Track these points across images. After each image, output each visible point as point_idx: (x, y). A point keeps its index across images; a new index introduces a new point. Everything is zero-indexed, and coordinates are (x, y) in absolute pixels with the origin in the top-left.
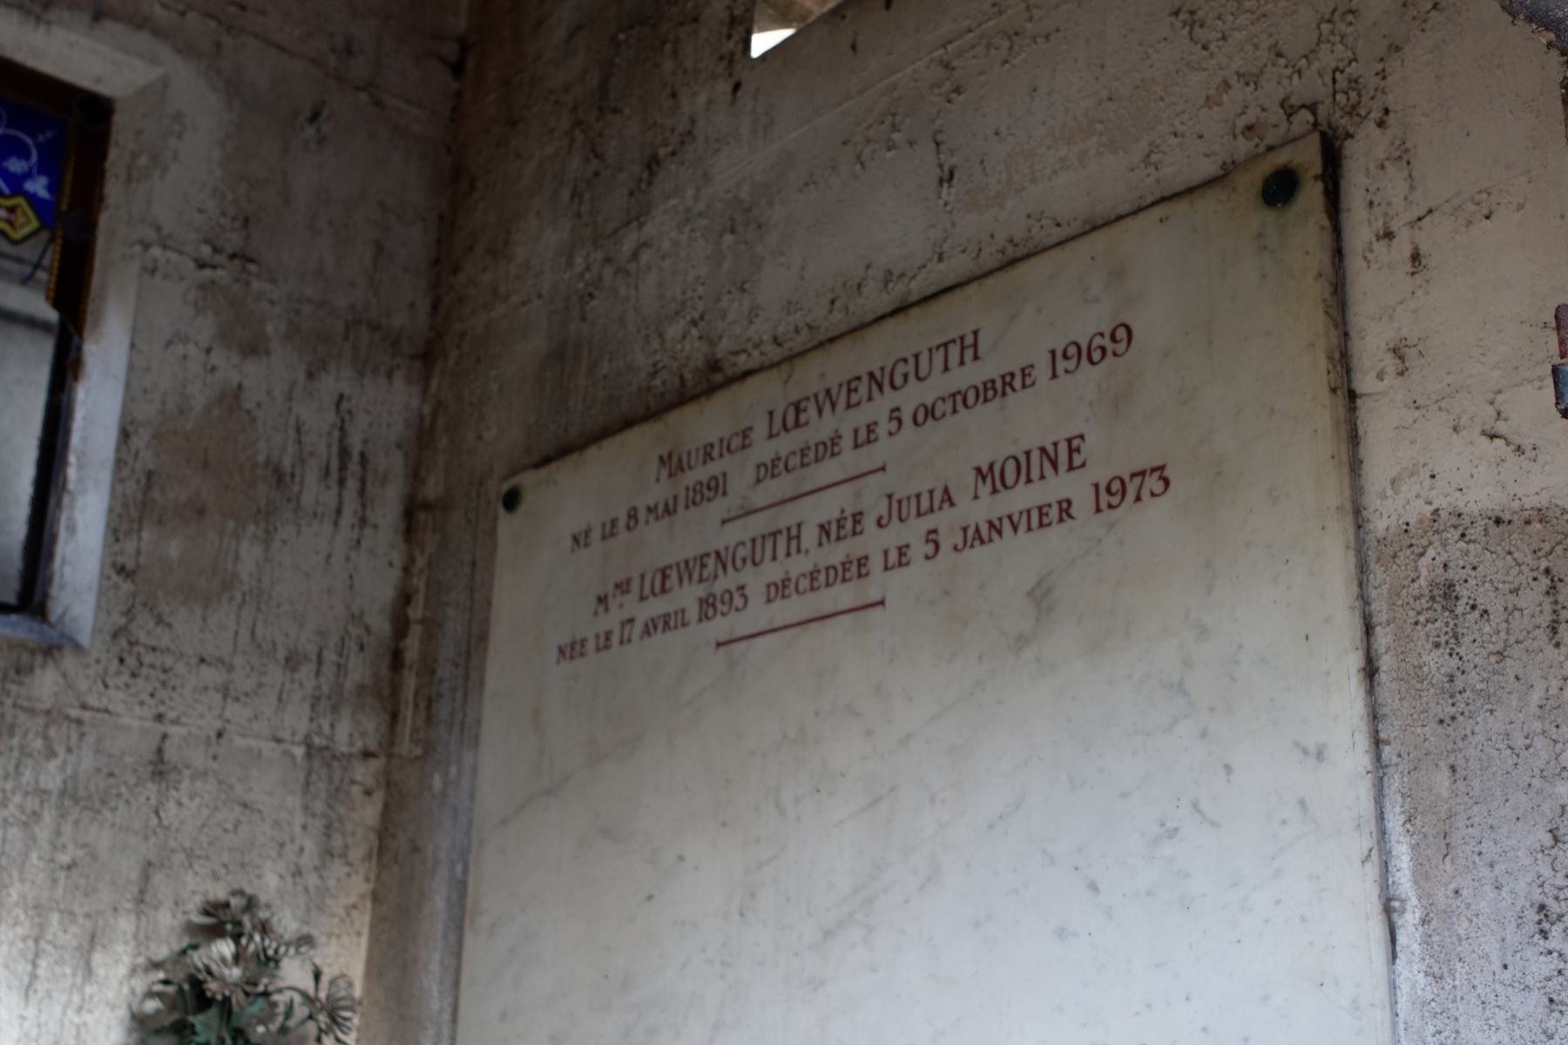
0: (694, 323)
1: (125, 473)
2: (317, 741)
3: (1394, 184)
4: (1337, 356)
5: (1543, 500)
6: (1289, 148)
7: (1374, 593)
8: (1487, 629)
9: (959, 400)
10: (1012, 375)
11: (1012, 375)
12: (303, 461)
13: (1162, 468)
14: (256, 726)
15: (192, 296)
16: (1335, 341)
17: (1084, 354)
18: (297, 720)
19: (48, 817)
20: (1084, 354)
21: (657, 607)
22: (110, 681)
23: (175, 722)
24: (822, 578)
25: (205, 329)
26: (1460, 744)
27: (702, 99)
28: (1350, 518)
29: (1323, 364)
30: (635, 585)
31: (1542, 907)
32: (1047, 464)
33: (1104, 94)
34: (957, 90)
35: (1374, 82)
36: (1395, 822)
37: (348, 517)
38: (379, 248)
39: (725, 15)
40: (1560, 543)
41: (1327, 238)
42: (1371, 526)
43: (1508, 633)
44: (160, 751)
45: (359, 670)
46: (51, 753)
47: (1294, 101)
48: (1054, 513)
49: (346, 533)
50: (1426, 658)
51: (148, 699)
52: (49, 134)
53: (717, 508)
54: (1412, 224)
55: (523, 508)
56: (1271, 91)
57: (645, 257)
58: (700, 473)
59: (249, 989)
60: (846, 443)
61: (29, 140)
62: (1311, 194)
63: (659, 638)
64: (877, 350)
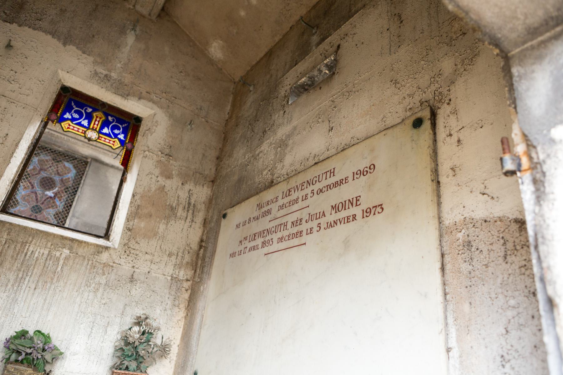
0: (269, 171)
1: (132, 205)
2: (174, 276)
3: (452, 121)
4: (434, 170)
5: (500, 214)
6: (421, 112)
7: (445, 244)
8: (482, 257)
9: (329, 187)
10: (343, 180)
11: (343, 180)
12: (178, 205)
13: (381, 205)
14: (159, 271)
15: (155, 164)
16: (433, 166)
17: (362, 173)
18: (170, 270)
19: (101, 290)
20: (362, 173)
21: (253, 244)
22: (122, 257)
23: (137, 268)
24: (291, 237)
25: (157, 172)
26: (473, 295)
27: (277, 116)
28: (437, 220)
29: (429, 173)
30: (248, 238)
31: (502, 356)
32: (350, 204)
33: (372, 104)
34: (335, 107)
35: (446, 93)
36: (450, 320)
37: (189, 219)
38: (204, 155)
39: (283, 95)
40: (507, 228)
41: (432, 136)
42: (444, 223)
43: (489, 258)
44: (132, 275)
45: (187, 258)
46: (104, 274)
47: (423, 100)
48: (351, 218)
49: (188, 224)
50: (461, 266)
51: (131, 262)
52: (126, 125)
53: (269, 217)
54: (457, 132)
55: (227, 218)
56: (417, 98)
57: (260, 155)
58: (266, 209)
59: (140, 341)
60: (300, 200)
61: (120, 126)
62: (427, 124)
63: (252, 252)
64: (309, 175)
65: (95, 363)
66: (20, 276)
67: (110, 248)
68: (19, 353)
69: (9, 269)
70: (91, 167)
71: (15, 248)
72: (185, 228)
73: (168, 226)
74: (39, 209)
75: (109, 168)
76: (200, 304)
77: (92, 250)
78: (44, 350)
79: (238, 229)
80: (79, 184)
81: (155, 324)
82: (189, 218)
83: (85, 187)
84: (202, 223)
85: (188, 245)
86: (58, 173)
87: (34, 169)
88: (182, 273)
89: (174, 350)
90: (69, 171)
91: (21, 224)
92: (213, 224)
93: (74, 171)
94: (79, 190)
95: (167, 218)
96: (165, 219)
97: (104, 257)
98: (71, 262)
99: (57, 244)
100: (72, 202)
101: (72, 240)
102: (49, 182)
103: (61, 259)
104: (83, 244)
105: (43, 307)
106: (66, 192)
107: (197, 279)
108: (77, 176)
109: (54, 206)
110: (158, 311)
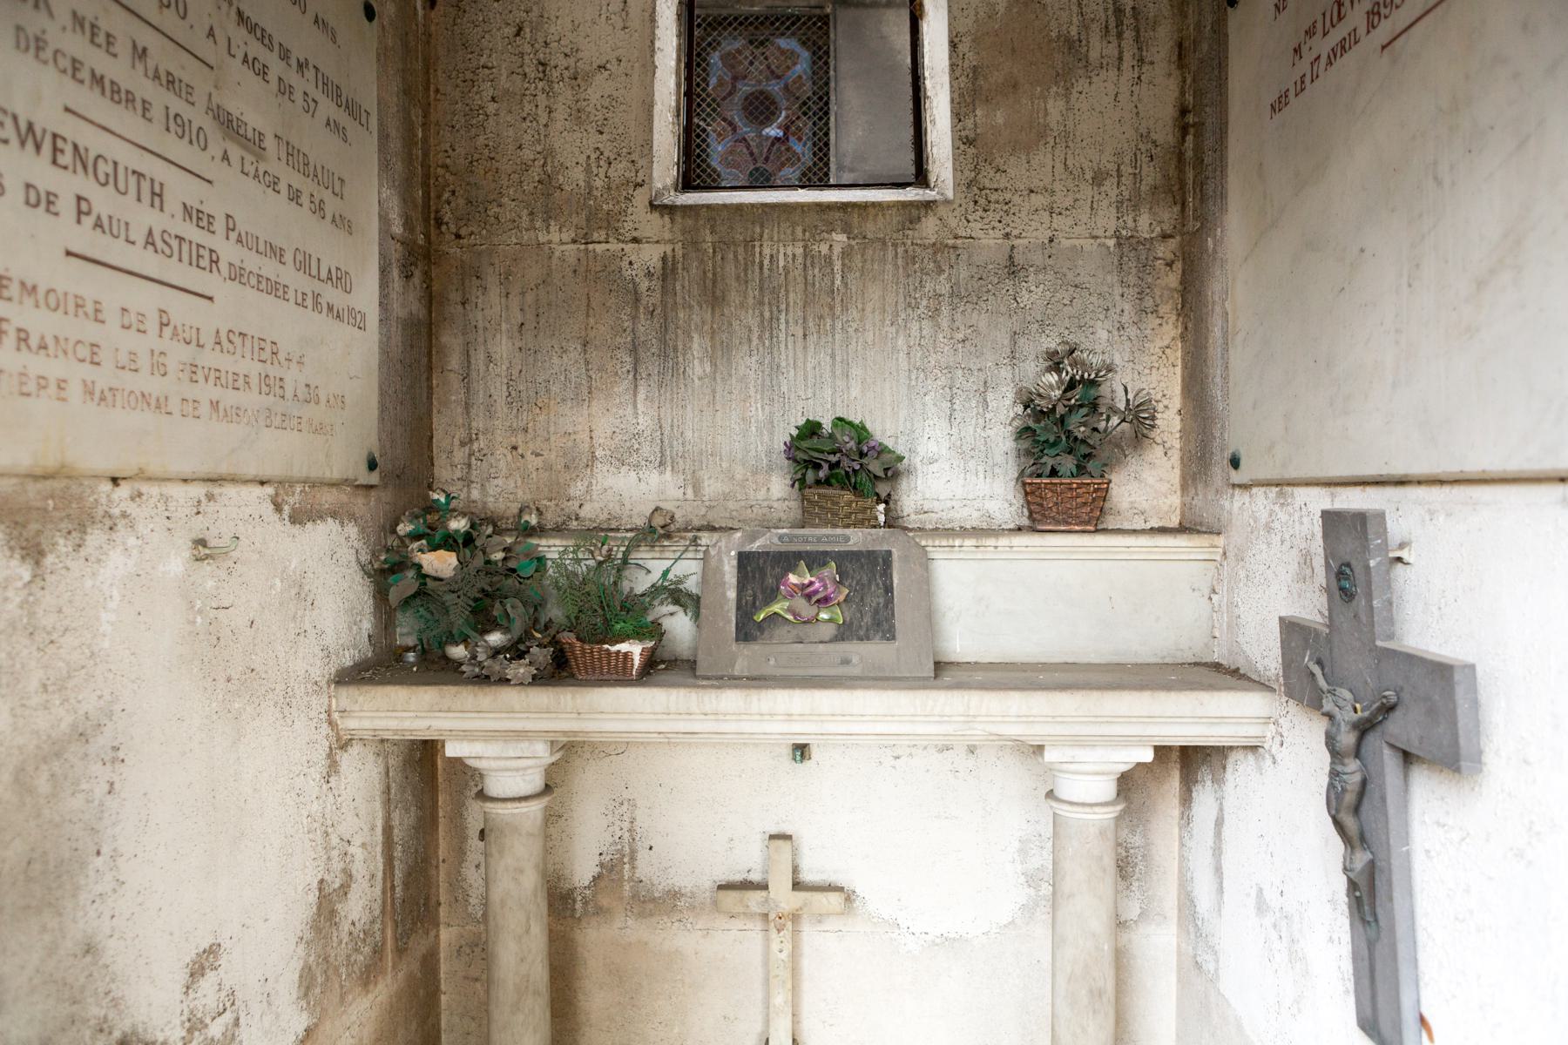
12: (1087, 28)
18: (1107, 220)
19: (945, 310)
23: (1018, 237)
30: (1319, 26)
44: (1011, 257)
45: (1151, 175)
46: (940, 271)
49: (1128, 74)
63: (1339, 63)
65: (981, 476)
66: (767, 315)
67: (934, 202)
68: (817, 467)
69: (742, 305)
70: (840, 29)
71: (736, 257)
72: (1124, 88)
73: (1073, 99)
74: (762, 175)
75: (882, 10)
76: (1214, 288)
77: (896, 218)
78: (862, 455)
79: (1284, 14)
80: (827, 84)
81: (1096, 360)
82: (1127, 56)
83: (842, 84)
84: (1175, 58)
85: (1145, 137)
86: (773, 72)
87: (721, 83)
88: (1144, 220)
89: (1169, 422)
90: (792, 56)
91: (728, 201)
92: (1205, 47)
93: (805, 54)
94: (833, 98)
95: (1064, 78)
96: (1056, 83)
97: (929, 227)
98: (858, 259)
99: (816, 227)
100: (827, 134)
101: (844, 207)
102: (762, 103)
103: (835, 258)
104: (872, 211)
105: (833, 372)
106: (805, 114)
107: (1193, 225)
108: (814, 63)
109: (794, 158)
110: (1104, 335)
